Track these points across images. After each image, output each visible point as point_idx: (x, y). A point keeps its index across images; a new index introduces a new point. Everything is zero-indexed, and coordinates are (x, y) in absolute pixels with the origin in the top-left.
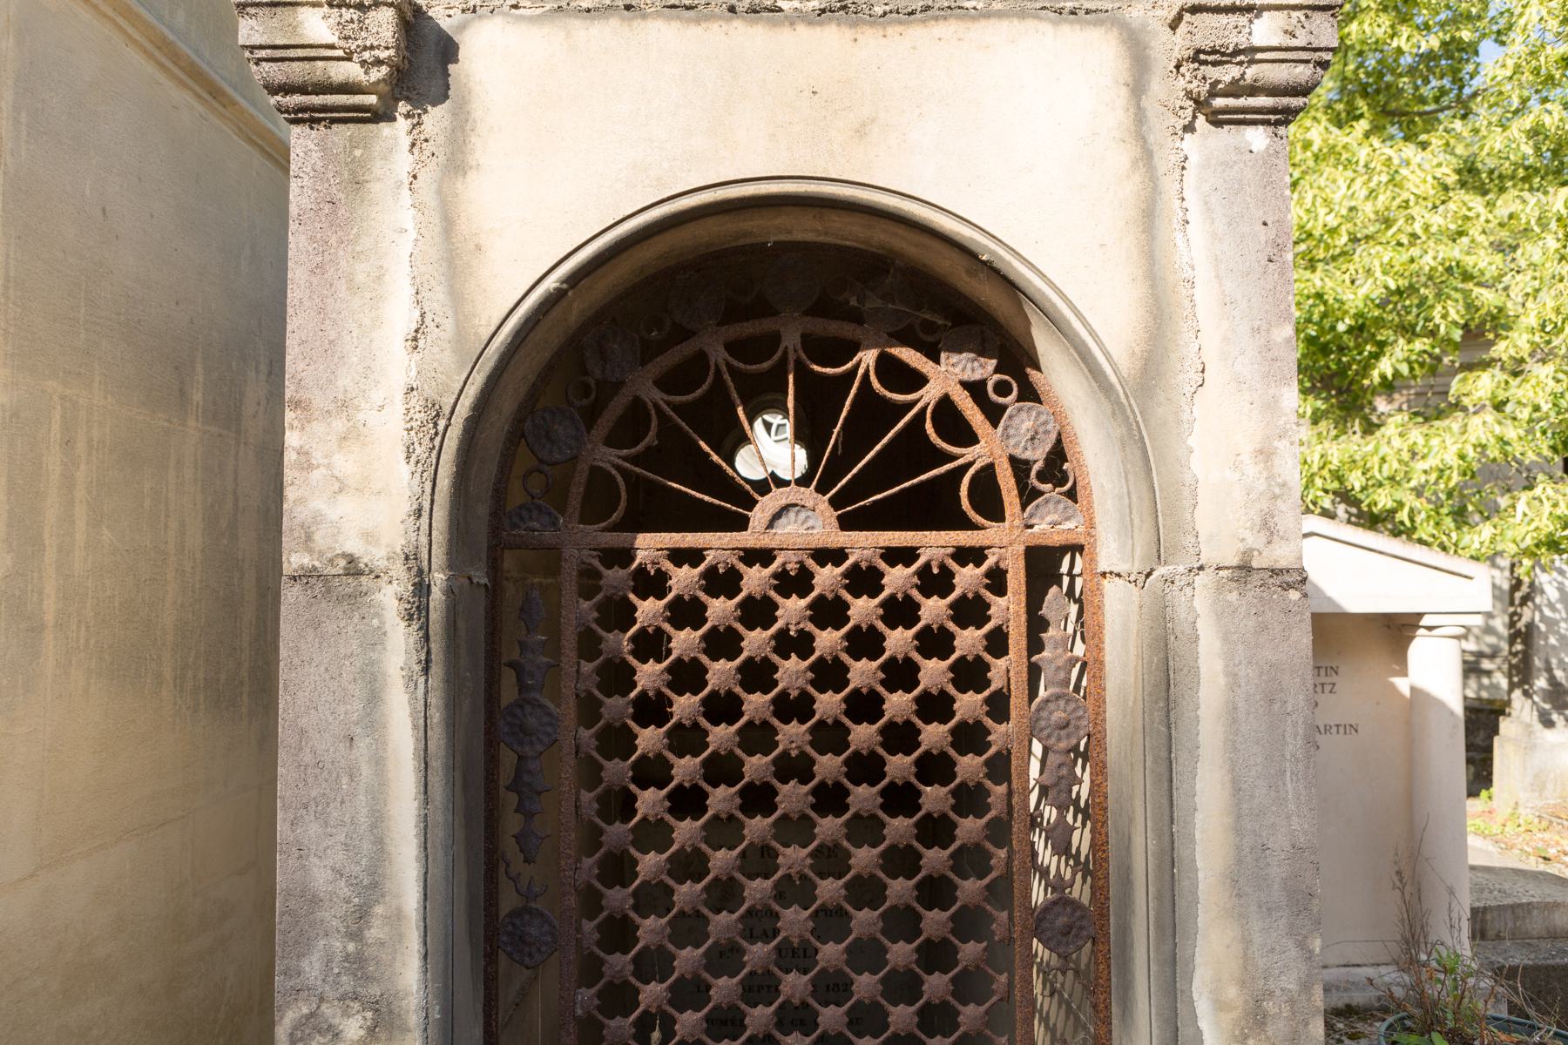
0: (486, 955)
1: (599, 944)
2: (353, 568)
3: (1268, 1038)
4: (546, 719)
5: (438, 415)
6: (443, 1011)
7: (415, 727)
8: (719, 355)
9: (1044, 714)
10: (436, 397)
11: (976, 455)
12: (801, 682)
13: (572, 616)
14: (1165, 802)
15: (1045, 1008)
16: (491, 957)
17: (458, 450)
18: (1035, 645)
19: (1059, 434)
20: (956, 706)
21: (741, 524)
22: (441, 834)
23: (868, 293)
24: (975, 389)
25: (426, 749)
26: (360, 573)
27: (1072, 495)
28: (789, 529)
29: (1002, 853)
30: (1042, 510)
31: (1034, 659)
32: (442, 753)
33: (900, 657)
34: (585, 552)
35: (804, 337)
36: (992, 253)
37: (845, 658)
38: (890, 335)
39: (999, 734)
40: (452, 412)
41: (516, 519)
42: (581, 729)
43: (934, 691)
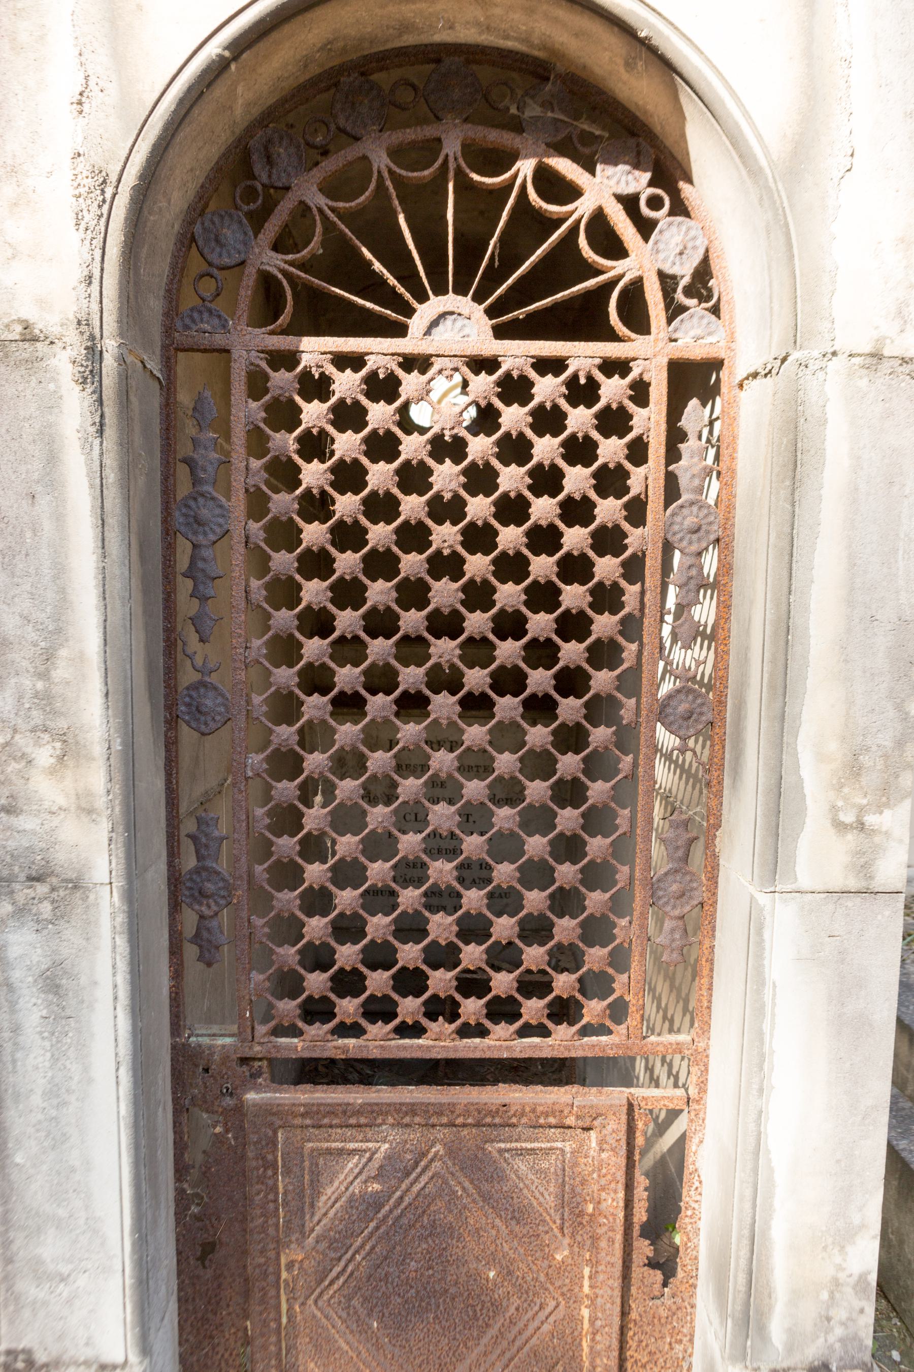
0: (166, 722)
1: (269, 827)
2: (29, 336)
3: (861, 787)
4: (218, 511)
5: (104, 182)
6: (124, 743)
7: (92, 486)
8: (381, 161)
9: (678, 519)
10: (103, 165)
11: (624, 269)
12: (454, 485)
13: (242, 414)
14: (785, 573)
15: (654, 1009)
16: (172, 722)
17: (126, 219)
18: (672, 455)
19: (707, 251)
20: (596, 511)
21: (400, 331)
22: (118, 585)
23: (529, 101)
24: (630, 203)
25: (102, 507)
26: (35, 339)
27: (716, 311)
28: (446, 336)
29: (634, 647)
30: (687, 324)
31: (671, 468)
32: (118, 510)
33: (547, 463)
34: (254, 353)
35: (464, 146)
36: (651, 26)
37: (495, 463)
38: (548, 145)
39: (635, 538)
40: (119, 181)
41: (188, 321)
42: (251, 522)
43: (577, 497)
